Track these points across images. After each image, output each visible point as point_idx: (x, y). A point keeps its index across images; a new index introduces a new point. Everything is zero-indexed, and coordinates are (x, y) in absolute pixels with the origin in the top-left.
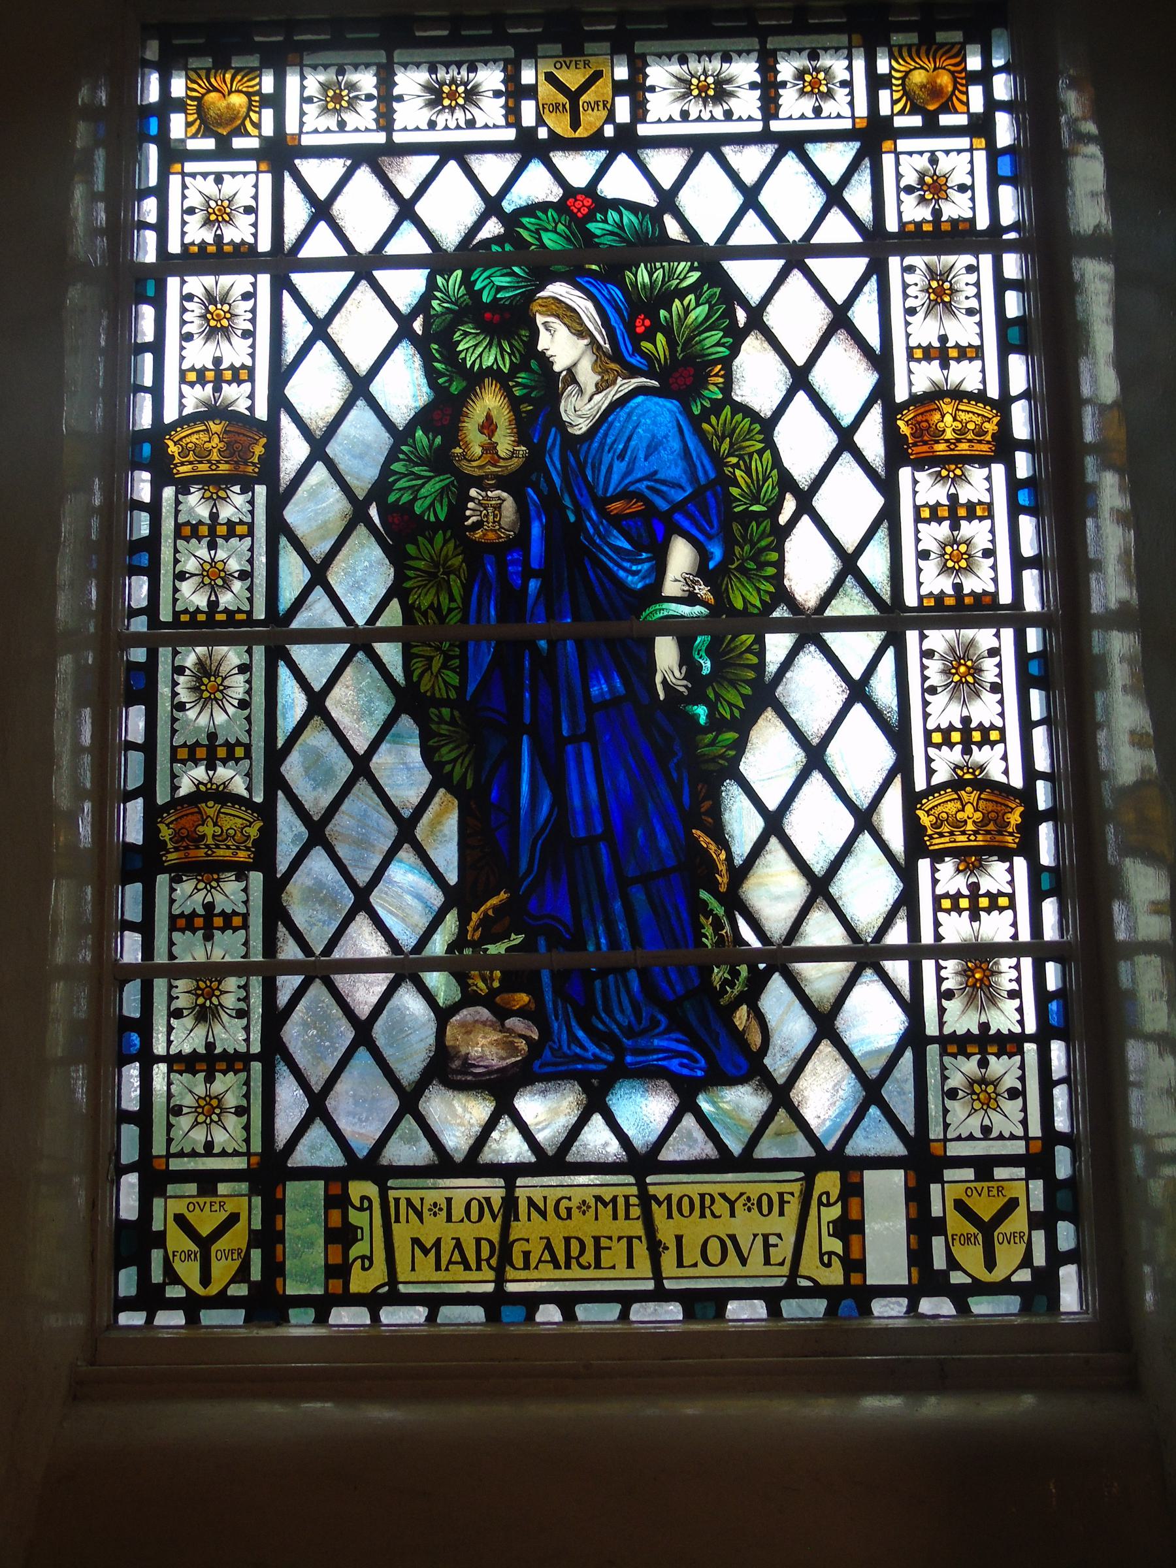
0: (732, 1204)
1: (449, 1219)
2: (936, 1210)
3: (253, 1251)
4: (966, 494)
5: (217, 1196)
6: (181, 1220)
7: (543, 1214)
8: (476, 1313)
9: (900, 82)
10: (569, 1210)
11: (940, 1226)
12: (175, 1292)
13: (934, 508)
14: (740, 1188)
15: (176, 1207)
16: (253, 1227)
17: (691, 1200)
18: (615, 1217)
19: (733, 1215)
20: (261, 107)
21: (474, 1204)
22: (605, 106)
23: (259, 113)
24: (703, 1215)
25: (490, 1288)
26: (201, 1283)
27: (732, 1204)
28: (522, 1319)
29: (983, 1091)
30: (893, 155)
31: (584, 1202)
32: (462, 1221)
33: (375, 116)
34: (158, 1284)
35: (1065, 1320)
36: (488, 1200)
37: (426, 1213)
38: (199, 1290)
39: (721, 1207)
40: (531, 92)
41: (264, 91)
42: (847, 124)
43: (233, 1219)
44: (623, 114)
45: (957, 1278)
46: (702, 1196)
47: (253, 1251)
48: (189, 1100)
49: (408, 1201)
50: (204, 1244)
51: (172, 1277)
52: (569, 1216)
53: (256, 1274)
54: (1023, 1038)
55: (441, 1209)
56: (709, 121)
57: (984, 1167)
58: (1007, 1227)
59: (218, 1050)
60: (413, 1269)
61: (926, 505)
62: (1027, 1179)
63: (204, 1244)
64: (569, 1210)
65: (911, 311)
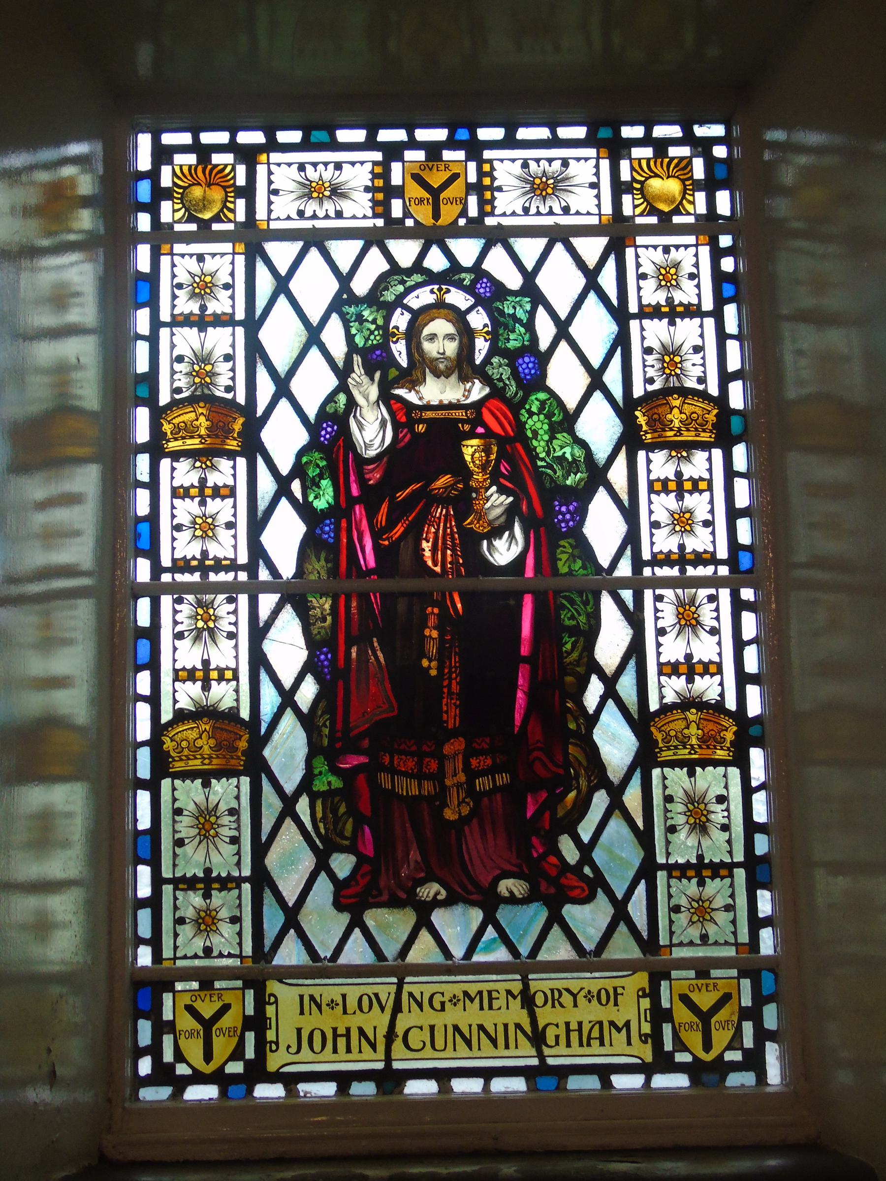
0: (575, 996)
1: (345, 1012)
2: (665, 1004)
3: (247, 1034)
4: (688, 471)
5: (711, 978)
6: (685, 999)
7: (420, 1005)
8: (518, 1084)
9: (179, 196)
10: (443, 1004)
11: (667, 1015)
12: (682, 1057)
13: (665, 482)
14: (585, 984)
15: (681, 987)
16: (743, 1004)
17: (606, 990)
18: (482, 1008)
19: (575, 1005)
20: (694, 190)
21: (365, 998)
22: (461, 202)
23: (693, 195)
24: (553, 1006)
25: (380, 1066)
26: (205, 1060)
27: (575, 996)
28: (554, 1088)
29: (702, 911)
30: (695, 243)
31: (454, 996)
32: (354, 1013)
33: (371, 204)
34: (169, 1063)
35: (769, 1089)
36: (376, 995)
37: (324, 1006)
38: (702, 1055)
39: (567, 999)
40: (399, 192)
41: (238, 184)
42: (594, 220)
43: (726, 998)
44: (473, 211)
45: (182, 1069)
46: (552, 990)
47: (247, 1034)
48: (684, 902)
49: (312, 998)
50: (705, 1017)
51: (680, 1045)
52: (443, 1009)
53: (250, 1054)
54: (731, 866)
55: (337, 1004)
56: (547, 214)
57: (703, 969)
58: (723, 1015)
59: (214, 875)
60: (455, 1050)
61: (658, 480)
62: (738, 978)
63: (705, 1017)
64: (443, 1004)
65: (697, 349)
